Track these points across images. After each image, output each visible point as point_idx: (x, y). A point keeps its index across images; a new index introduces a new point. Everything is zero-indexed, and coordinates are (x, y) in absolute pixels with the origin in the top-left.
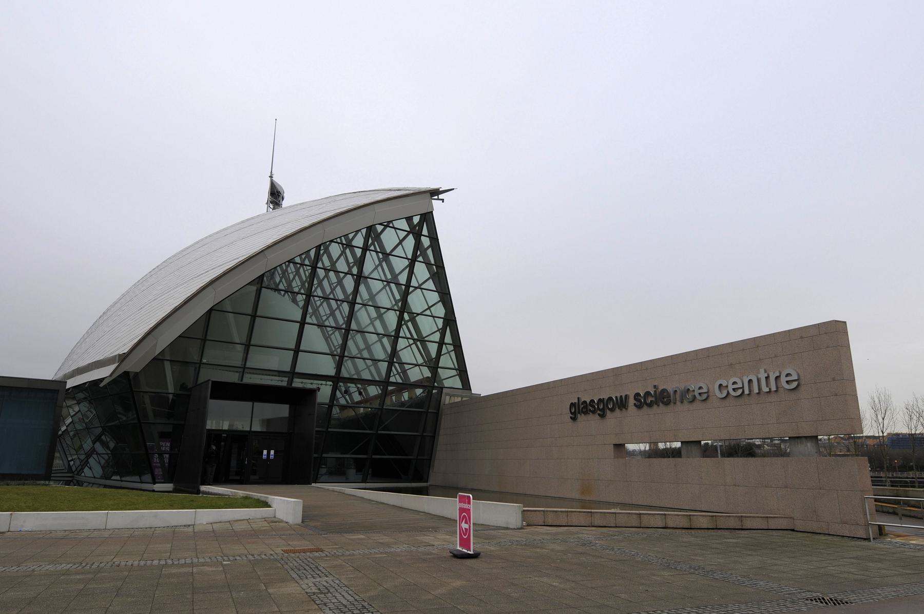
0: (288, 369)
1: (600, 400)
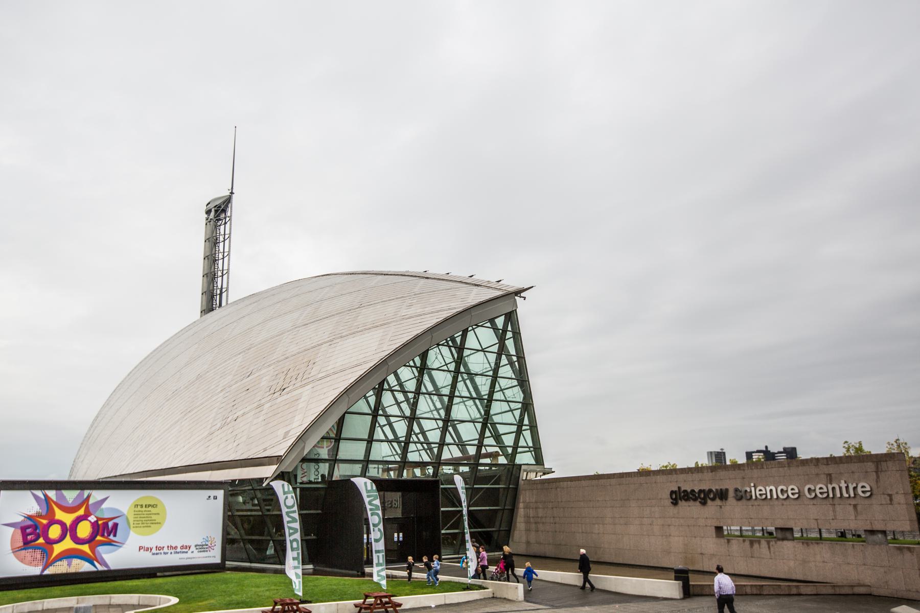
0: (362, 458)
1: (700, 491)
